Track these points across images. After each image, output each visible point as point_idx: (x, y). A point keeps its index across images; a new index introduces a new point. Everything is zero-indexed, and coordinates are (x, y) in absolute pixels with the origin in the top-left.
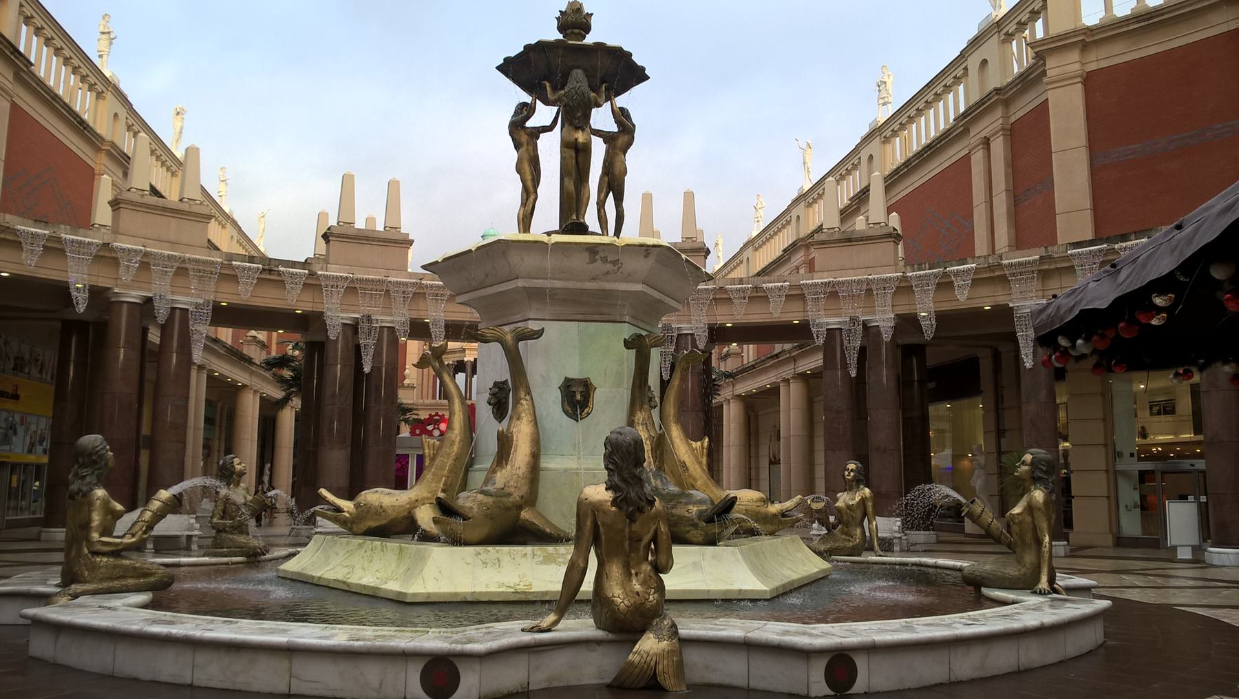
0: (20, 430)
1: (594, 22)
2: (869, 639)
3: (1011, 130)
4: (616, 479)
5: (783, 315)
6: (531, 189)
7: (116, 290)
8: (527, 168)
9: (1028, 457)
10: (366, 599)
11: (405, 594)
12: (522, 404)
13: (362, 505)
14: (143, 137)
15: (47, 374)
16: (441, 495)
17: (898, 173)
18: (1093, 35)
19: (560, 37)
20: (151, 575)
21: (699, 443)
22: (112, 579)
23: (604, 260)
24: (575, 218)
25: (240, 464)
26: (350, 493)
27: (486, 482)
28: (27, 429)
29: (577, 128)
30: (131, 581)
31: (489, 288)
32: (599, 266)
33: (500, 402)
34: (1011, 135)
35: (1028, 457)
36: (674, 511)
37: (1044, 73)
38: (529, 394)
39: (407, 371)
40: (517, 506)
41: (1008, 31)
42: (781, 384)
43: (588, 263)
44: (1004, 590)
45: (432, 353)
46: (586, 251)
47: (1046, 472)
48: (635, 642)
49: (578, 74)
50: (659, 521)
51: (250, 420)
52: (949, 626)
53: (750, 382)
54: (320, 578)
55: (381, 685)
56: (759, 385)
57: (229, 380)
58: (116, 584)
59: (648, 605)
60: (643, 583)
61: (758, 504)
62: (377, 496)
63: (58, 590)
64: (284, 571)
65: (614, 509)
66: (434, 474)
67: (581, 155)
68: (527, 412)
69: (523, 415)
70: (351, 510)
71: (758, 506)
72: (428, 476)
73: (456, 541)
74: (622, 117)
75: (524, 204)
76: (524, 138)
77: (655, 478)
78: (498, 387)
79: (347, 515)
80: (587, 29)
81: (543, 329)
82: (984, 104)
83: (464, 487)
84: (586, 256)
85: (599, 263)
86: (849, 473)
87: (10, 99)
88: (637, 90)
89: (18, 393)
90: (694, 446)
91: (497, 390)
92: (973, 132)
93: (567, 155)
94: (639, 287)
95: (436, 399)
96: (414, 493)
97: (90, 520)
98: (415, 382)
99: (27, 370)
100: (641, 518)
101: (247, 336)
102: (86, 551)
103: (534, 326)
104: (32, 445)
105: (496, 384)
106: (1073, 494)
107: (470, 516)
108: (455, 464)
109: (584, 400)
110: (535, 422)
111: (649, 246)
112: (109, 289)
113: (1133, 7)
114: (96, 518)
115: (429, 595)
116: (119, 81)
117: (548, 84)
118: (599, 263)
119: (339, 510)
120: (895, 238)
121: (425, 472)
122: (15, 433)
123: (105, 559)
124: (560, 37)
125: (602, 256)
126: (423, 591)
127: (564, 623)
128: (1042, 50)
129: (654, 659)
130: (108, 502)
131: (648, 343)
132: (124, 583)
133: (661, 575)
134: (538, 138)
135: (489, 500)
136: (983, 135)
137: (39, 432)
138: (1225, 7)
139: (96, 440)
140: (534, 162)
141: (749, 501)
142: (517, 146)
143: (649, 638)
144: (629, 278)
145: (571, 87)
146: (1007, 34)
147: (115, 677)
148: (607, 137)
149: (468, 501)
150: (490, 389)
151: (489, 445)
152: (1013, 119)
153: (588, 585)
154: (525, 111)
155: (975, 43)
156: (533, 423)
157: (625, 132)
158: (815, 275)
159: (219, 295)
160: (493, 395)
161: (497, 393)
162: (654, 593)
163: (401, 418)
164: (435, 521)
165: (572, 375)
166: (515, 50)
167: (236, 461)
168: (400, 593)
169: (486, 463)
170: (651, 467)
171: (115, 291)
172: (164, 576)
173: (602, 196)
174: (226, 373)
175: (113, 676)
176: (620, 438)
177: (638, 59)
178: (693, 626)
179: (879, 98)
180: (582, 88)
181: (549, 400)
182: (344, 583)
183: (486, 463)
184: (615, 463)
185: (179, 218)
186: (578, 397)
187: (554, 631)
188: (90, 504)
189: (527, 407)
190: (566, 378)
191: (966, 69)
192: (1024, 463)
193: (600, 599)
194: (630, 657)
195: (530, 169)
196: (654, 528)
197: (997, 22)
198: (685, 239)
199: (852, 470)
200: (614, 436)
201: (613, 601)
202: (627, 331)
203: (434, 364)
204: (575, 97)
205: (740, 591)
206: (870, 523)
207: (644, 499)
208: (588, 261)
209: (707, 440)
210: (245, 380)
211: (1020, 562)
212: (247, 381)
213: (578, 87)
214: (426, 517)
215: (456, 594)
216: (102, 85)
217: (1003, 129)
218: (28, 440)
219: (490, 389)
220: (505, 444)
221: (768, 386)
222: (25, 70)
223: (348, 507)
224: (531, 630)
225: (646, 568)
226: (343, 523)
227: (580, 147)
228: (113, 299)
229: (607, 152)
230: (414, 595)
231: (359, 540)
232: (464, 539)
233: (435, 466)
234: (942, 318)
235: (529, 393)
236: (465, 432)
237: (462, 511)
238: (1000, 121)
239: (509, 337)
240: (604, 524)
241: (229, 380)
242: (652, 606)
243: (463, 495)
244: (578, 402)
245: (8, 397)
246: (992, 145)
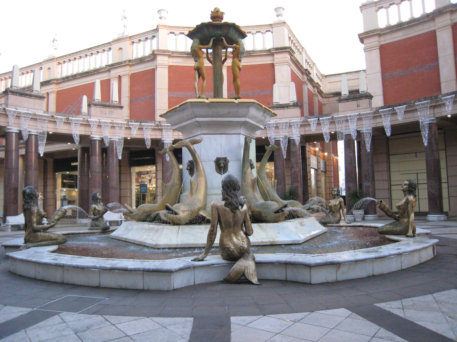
2: (104, 266)
5: (316, 131)
7: (8, 127)
10: (269, 247)
18: (383, 31)
44: (397, 236)
52: (376, 252)
103: (197, 138)
112: (6, 127)
120: (300, 106)
127: (208, 258)
129: (244, 268)
133: (248, 237)
136: (119, 74)
147: (288, 281)
153: (217, 241)
158: (339, 113)
159: (49, 129)
175: (286, 281)
178: (262, 257)
187: (205, 260)
190: (217, 157)
193: (223, 247)
224: (195, 260)
244: (222, 167)
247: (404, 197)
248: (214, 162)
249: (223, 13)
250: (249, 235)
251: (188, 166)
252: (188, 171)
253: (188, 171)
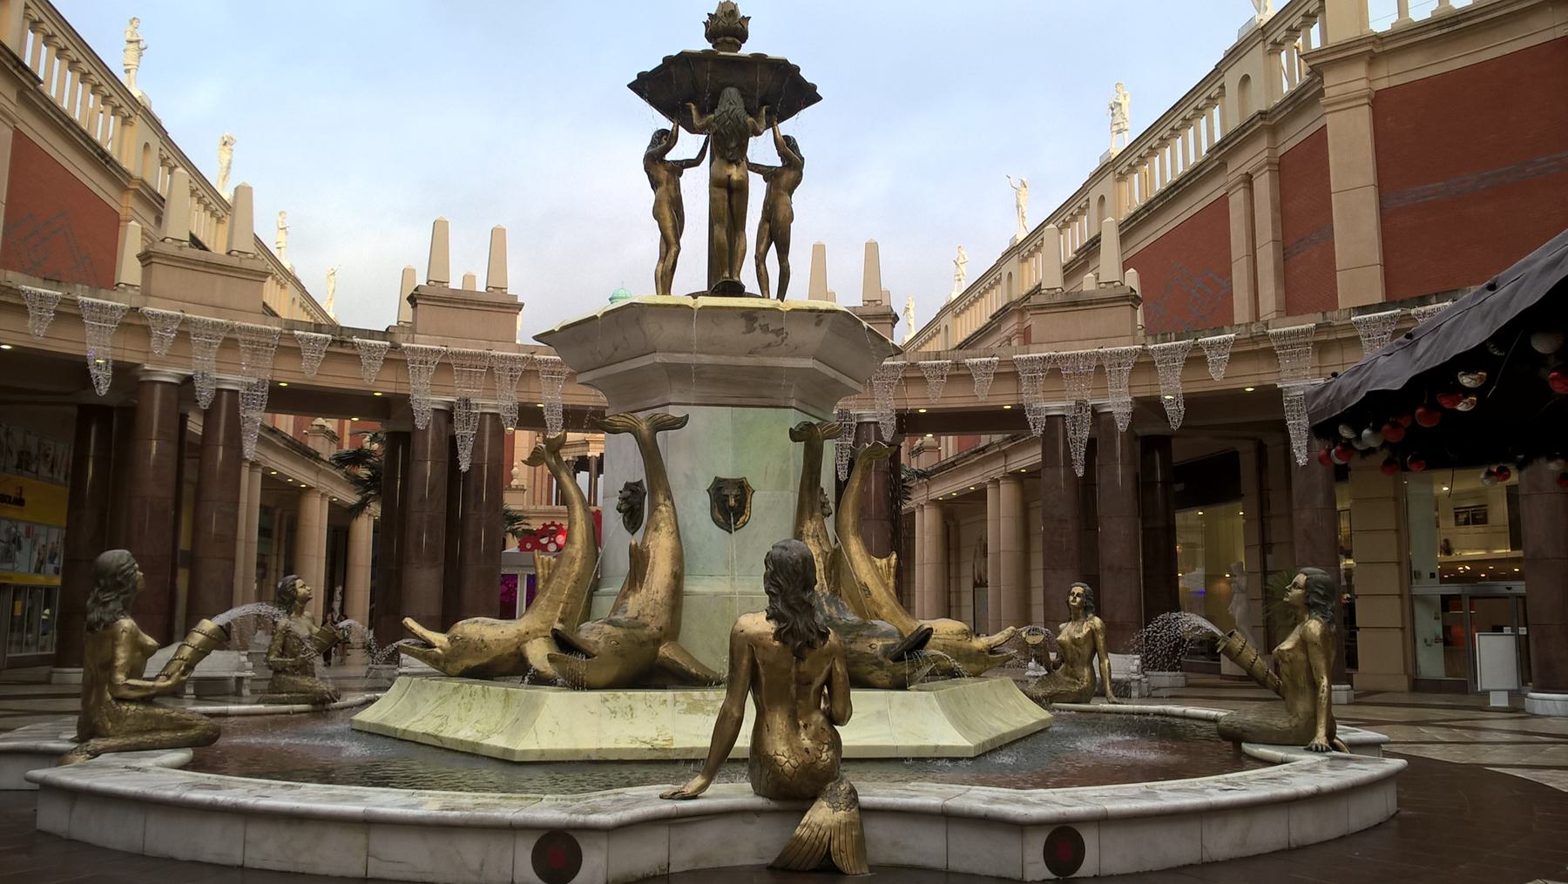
0: (26, 544)
1: (752, 28)
2: (1100, 808)
3: (1279, 165)
4: (779, 605)
5: (991, 399)
6: (672, 239)
7: (147, 367)
8: (666, 212)
9: (1301, 578)
11: (512, 752)
12: (660, 511)
13: (458, 638)
14: (181, 173)
15: (59, 473)
16: (558, 626)
17: (1137, 219)
18: (1383, 45)
19: (709, 46)
20: (191, 727)
21: (884, 561)
22: (141, 732)
23: (765, 329)
24: (728, 275)
25: (303, 586)
26: (443, 624)
27: (615, 610)
28: (34, 543)
29: (730, 162)
30: (165, 735)
31: (619, 364)
32: (758, 337)
33: (633, 508)
34: (1279, 171)
35: (1301, 578)
36: (853, 646)
37: (1321, 93)
38: (669, 499)
39: (515, 469)
40: (654, 640)
41: (1276, 39)
42: (988, 486)
43: (744, 333)
44: (1271, 746)
45: (547, 447)
46: (742, 317)
47: (1323, 597)
48: (804, 812)
49: (732, 93)
50: (834, 659)
51: (316, 531)
52: (1201, 791)
53: (949, 484)
54: (405, 731)
55: (482, 866)
56: (960, 487)
57: (290, 480)
58: (147, 738)
59: (821, 765)
60: (814, 738)
61: (960, 637)
62: (477, 627)
63: (74, 746)
64: (360, 722)
65: (777, 643)
66: (549, 600)
67: (735, 196)
68: (667, 521)
69: (662, 525)
70: (444, 645)
71: (959, 640)
72: (541, 601)
73: (577, 684)
74: (787, 148)
75: (663, 258)
76: (663, 174)
77: (829, 605)
78: (630, 490)
79: (439, 651)
80: (743, 36)
81: (687, 416)
82: (1245, 131)
83: (587, 615)
84: (741, 324)
85: (758, 332)
86: (1075, 598)
87: (12, 126)
88: (806, 114)
89: (23, 496)
90: (878, 564)
91: (629, 493)
92: (1231, 167)
93: (717, 196)
94: (809, 363)
95: (552, 504)
96: (524, 624)
97: (113, 658)
98: (525, 483)
99: (34, 468)
100: (811, 656)
101: (312, 425)
102: (109, 696)
103: (675, 412)
104: (41, 562)
105: (627, 486)
106: (1358, 625)
107: (595, 652)
108: (576, 587)
109: (739, 506)
110: (677, 533)
111: (821, 311)
112: (138, 365)
113: (1434, 8)
114: (122, 655)
115: (543, 752)
116: (150, 102)
117: (693, 107)
118: (758, 332)
119: (429, 645)
120: (1132, 300)
121: (538, 597)
122: (19, 548)
123: (133, 707)
124: (709, 46)
125: (762, 324)
126: (535, 747)
127: (713, 788)
128: (1319, 64)
129: (828, 833)
130: (137, 635)
131: (820, 434)
132: (157, 737)
133: (836, 727)
134: (681, 174)
135: (619, 632)
136: (1244, 170)
137: (50, 546)
138: (1550, 9)
139: (121, 556)
140: (676, 205)
141: (947, 634)
142: (655, 185)
143: (821, 807)
144: (796, 352)
145: (723, 110)
146: (1274, 43)
147: (146, 856)
148: (769, 174)
149: (592, 633)
150: (621, 492)
151: (619, 563)
152: (1282, 151)
153: (744, 740)
154: (664, 141)
155: (1234, 54)
156: (674, 535)
157: (791, 167)
158: (1032, 347)
159: (278, 373)
160: (624, 499)
161: (629, 497)
162: (828, 750)
163: (508, 529)
164: (551, 659)
165: (724, 475)
166: (652, 63)
167: (299, 582)
168: (506, 750)
169: (615, 585)
170: (824, 591)
171: (146, 368)
172: (208, 729)
173: (762, 248)
174: (286, 472)
175: (143, 855)
176: (785, 554)
177: (807, 75)
178: (877, 792)
179: (1113, 124)
180: (737, 111)
181: (695, 506)
182: (436, 737)
183: (615, 585)
184: (778, 586)
185: (227, 276)
186: (732, 502)
187: (702, 797)
188: (114, 638)
189: (666, 514)
190: (716, 477)
191: (1222, 87)
192: (1295, 586)
193: (759, 757)
194: (798, 831)
195: (670, 214)
196: (827, 667)
197: (1262, 28)
198: (867, 303)
199: (1078, 595)
200: (778, 551)
201: (776, 760)
202: (793, 419)
203: (549, 460)
204: (727, 123)
205: (937, 747)
206: (1101, 661)
207: (814, 631)
208: (745, 330)
209: (895, 556)
210: (310, 481)
211: (1290, 710)
212: (313, 482)
213: (731, 110)
214: (539, 653)
215: (577, 751)
216: (129, 108)
217: (1269, 163)
218: (35, 556)
219: (621, 492)
220: (639, 561)
221: (972, 488)
222: (32, 88)
223: (440, 641)
224: (672, 797)
225: (818, 718)
226: (434, 661)
227: (734, 186)
228: (143, 379)
229: (769, 192)
230: (524, 752)
231: (454, 683)
232: (587, 682)
233: (550, 590)
235: (669, 497)
236: (588, 547)
237: (585, 647)
238: (1266, 153)
239: (644, 427)
240: (764, 663)
241: (290, 480)
242: (825, 766)
243: (586, 625)
244: (732, 508)
245: (10, 503)
246: (1256, 184)
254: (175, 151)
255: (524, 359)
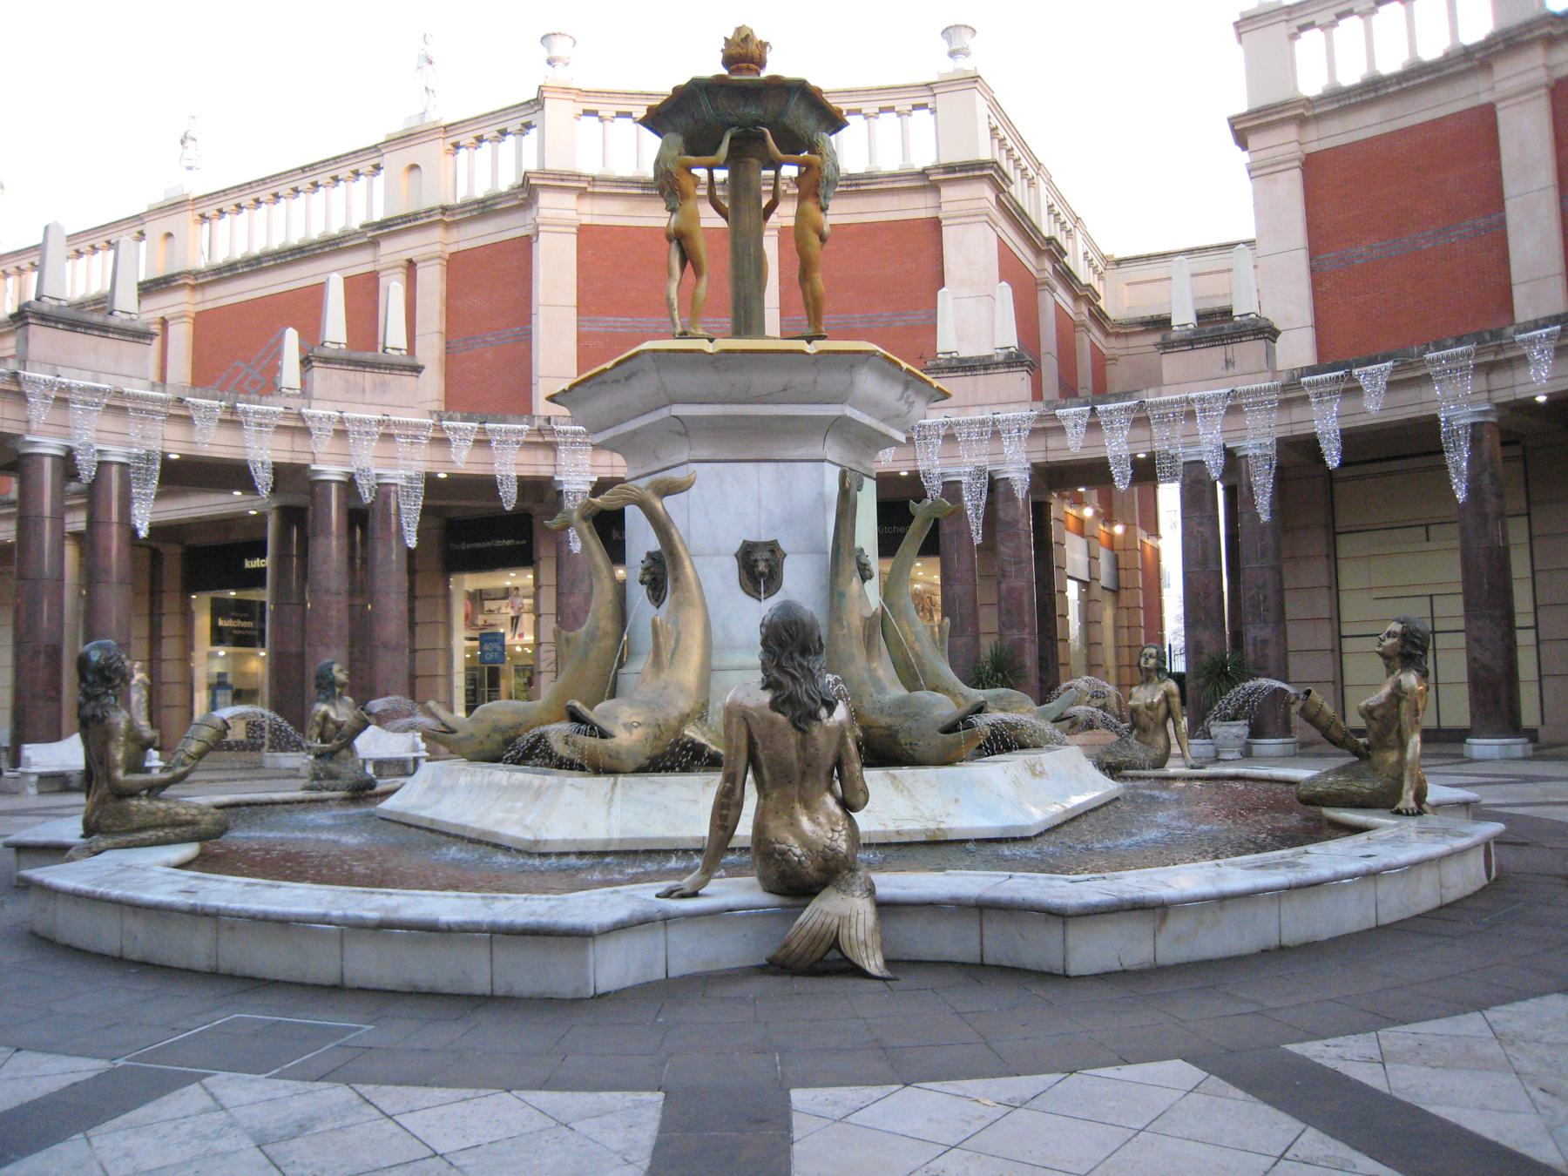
2: (358, 913)
5: (1085, 451)
7: (29, 438)
18: (1313, 107)
19: (725, 72)
44: (1363, 810)
80: (761, 63)
103: (677, 475)
112: (19, 436)
117: (766, 130)
120: (1028, 366)
124: (725, 72)
127: (714, 886)
129: (836, 922)
133: (852, 814)
146: (203, 216)
147: (987, 966)
153: (744, 828)
158: (1164, 389)
159: (168, 444)
175: (982, 965)
178: (897, 883)
187: (705, 895)
190: (744, 541)
193: (764, 850)
224: (669, 894)
234: (1352, 440)
244: (762, 574)
247: (1385, 676)
248: (736, 556)
249: (763, 46)
250: (855, 809)
251: (646, 569)
252: (645, 587)
253: (645, 587)
254: (484, 121)
255: (379, 423)
